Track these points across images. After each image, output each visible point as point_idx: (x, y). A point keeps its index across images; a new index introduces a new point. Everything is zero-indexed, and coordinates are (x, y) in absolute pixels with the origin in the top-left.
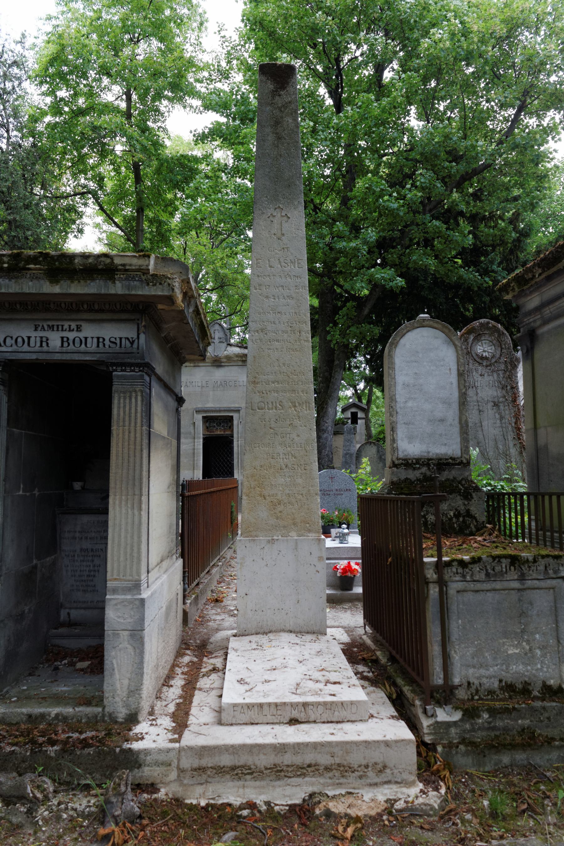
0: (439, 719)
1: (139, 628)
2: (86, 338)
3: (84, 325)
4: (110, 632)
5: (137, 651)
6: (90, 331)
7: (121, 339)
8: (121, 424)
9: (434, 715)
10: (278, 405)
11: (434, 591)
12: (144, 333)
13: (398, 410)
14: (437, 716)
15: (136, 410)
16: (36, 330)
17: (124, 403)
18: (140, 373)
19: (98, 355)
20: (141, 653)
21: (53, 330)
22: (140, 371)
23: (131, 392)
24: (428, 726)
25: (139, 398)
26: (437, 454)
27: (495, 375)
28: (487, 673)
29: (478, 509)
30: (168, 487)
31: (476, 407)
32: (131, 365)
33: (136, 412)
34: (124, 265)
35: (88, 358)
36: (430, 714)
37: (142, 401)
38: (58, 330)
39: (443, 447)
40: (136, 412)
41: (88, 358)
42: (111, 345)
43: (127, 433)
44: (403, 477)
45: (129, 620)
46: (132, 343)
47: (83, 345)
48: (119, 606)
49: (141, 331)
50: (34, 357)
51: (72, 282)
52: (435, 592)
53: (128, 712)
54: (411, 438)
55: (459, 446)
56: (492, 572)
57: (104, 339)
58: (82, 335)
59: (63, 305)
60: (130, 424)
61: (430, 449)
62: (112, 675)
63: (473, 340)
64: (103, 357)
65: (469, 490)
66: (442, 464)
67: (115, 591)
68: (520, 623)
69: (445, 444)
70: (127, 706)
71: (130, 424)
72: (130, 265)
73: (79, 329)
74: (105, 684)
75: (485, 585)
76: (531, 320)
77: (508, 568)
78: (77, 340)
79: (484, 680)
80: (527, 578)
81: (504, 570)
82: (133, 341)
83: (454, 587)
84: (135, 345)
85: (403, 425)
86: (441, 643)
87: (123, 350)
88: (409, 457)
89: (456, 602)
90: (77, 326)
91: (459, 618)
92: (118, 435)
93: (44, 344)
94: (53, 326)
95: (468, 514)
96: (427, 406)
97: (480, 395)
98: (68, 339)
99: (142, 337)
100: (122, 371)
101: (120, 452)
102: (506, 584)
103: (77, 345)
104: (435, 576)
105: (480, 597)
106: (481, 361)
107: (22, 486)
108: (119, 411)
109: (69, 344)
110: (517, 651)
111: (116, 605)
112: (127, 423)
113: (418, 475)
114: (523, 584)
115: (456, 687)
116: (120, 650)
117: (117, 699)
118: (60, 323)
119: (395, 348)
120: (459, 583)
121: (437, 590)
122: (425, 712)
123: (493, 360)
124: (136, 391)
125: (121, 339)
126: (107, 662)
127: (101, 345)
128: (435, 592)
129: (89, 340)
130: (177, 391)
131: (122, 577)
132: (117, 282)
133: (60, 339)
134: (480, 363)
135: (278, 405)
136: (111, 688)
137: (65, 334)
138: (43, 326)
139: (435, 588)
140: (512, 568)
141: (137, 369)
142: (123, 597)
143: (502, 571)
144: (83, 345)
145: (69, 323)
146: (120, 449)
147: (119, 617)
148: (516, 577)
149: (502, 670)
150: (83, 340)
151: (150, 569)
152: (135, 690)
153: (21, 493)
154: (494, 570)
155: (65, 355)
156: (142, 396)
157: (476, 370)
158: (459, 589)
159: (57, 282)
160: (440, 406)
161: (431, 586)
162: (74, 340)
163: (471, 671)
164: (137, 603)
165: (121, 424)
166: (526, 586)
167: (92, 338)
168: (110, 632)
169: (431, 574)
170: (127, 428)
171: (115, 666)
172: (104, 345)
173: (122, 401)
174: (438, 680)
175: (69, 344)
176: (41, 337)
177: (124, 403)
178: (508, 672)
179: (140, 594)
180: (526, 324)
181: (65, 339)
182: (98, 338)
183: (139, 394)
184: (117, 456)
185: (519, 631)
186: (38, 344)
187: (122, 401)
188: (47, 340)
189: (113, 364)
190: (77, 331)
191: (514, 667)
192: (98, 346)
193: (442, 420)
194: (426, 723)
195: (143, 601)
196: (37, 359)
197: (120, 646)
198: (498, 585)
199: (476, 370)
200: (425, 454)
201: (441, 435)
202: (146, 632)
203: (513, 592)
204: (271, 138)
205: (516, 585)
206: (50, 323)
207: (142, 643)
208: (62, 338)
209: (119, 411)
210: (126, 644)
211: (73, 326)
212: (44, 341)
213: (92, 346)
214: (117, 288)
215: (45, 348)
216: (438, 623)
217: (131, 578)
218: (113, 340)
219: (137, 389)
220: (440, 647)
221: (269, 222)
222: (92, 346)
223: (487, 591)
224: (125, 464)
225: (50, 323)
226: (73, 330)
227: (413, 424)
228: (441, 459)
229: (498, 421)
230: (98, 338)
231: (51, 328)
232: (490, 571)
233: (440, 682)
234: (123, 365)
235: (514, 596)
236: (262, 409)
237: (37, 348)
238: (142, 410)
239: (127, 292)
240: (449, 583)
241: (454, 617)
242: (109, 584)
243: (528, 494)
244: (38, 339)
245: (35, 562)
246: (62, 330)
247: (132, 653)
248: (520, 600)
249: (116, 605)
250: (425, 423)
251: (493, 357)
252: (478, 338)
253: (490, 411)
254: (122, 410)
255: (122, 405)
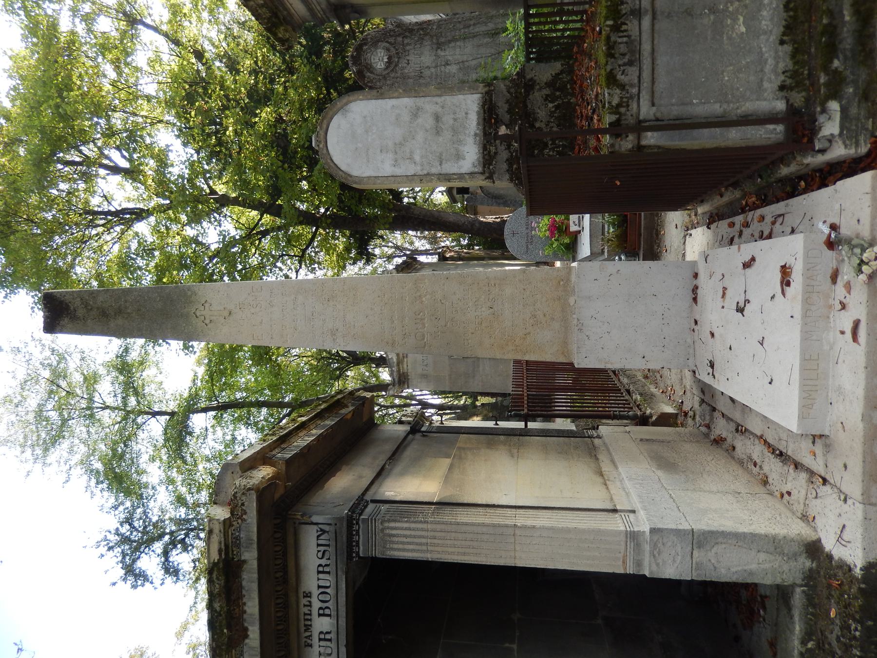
0: (836, 131)
1: (690, 536)
2: (319, 587)
3: (304, 588)
4: (694, 574)
5: (720, 540)
6: (311, 581)
7: (318, 545)
8: (424, 548)
9: (830, 140)
10: (419, 317)
11: (651, 139)
12: (310, 517)
13: (425, 172)
14: (832, 135)
15: (406, 529)
16: (311, 646)
17: (397, 543)
18: (360, 523)
19: (339, 573)
20: (724, 534)
21: (311, 625)
22: (357, 523)
23: (385, 535)
24: (846, 147)
25: (392, 525)
26: (478, 124)
27: (408, 48)
28: (770, 61)
29: (545, 72)
30: (512, 456)
31: (443, 68)
32: (350, 536)
33: (409, 529)
34: (220, 551)
35: (343, 586)
36: (827, 144)
37: (395, 521)
38: (310, 620)
39: (469, 116)
40: (409, 529)
41: (344, 586)
42: (327, 556)
43: (436, 541)
44: (505, 166)
45: (679, 549)
46: (324, 532)
47: (328, 590)
48: (660, 561)
49: (308, 521)
50: (343, 650)
51: (245, 612)
52: (652, 137)
53: (804, 555)
54: (459, 157)
55: (469, 96)
56: (627, 57)
57: (320, 565)
58: (315, 592)
59: (279, 614)
60: (423, 537)
61: (473, 133)
62: (751, 573)
63: (372, 73)
64: (342, 567)
65: (522, 84)
66: (489, 115)
67: (639, 564)
68: (701, 14)
69: (466, 114)
70: (795, 556)
71: (423, 537)
72: (220, 543)
73: (308, 595)
74: (765, 582)
75: (645, 67)
76: (318, 8)
77: (622, 34)
78: (322, 597)
79: (781, 66)
80: (637, 7)
81: (625, 39)
82: (321, 530)
83: (646, 110)
84: (326, 528)
85: (443, 166)
86: (725, 129)
87: (333, 543)
88: (481, 160)
89: (671, 109)
90: (304, 597)
91: (691, 103)
92: (438, 552)
93: (328, 636)
94: (305, 625)
95: (550, 84)
96: (420, 136)
97: (429, 64)
98: (320, 608)
99: (315, 519)
100: (358, 545)
101: (460, 550)
102: (646, 37)
103: (327, 598)
104: (631, 137)
105: (660, 71)
106: (394, 64)
107: (507, 645)
108: (408, 550)
109: (327, 608)
110: (741, 19)
111: (658, 565)
112: (424, 541)
113: (503, 148)
114: (647, 11)
115: (790, 106)
116: (719, 562)
117: (786, 568)
118: (302, 617)
119: (351, 176)
120: (641, 103)
121: (649, 134)
122: (823, 151)
123: (393, 51)
124: (382, 530)
125: (318, 545)
126: (734, 579)
127: (327, 569)
128: (652, 137)
129: (322, 583)
130: (403, 435)
131: (622, 554)
132: (243, 558)
133: (321, 618)
134: (396, 65)
135: (419, 317)
136: (769, 575)
137: (315, 612)
138: (306, 637)
139: (646, 137)
140: (624, 27)
141: (356, 527)
142: (647, 554)
143: (626, 43)
144: (328, 590)
145: (302, 606)
146: (457, 550)
147: (674, 561)
148: (636, 22)
149: (767, 40)
150: (321, 590)
151: (610, 507)
152: (774, 544)
153: (515, 646)
154: (624, 55)
155: (340, 613)
156: (389, 521)
157: (403, 68)
158: (650, 104)
159: (246, 630)
160: (420, 120)
161: (644, 142)
162: (322, 601)
163: (766, 85)
164: (655, 538)
165: (424, 548)
166: (649, 7)
167: (318, 579)
168: (694, 574)
169: (627, 144)
170: (429, 541)
171: (740, 568)
172: (326, 565)
173: (396, 546)
174: (775, 132)
175: (327, 608)
176: (320, 640)
177: (397, 543)
178: (771, 31)
179: (644, 532)
180: (325, 14)
181: (321, 612)
182: (319, 572)
183: (386, 525)
184: (464, 554)
185: (712, 17)
186: (328, 643)
187: (396, 546)
188: (321, 633)
189: (349, 557)
190: (310, 597)
191: (763, 22)
192: (328, 573)
193: (437, 118)
194: (839, 151)
195: (653, 531)
196: (346, 646)
197: (713, 561)
198: (646, 47)
199: (403, 68)
200: (478, 138)
201: (455, 120)
202: (697, 527)
203: (657, 27)
204: (120, 321)
205: (646, 22)
206: (303, 629)
207: (712, 533)
208: (320, 615)
209: (408, 550)
210: (711, 555)
211: (304, 601)
212: (324, 637)
213: (328, 580)
214: (250, 556)
215: (333, 636)
216: (696, 132)
217: (623, 544)
218: (320, 555)
219: (381, 527)
220: (731, 129)
221: (212, 324)
222: (328, 580)
223: (653, 63)
224: (475, 544)
225: (303, 629)
226: (310, 602)
227: (441, 154)
228: (484, 119)
229: (458, 43)
230: (319, 572)
231: (308, 628)
232: (626, 60)
233: (780, 128)
234: (351, 544)
235: (662, 25)
236: (424, 335)
237: (333, 645)
238: (406, 522)
239: (255, 546)
240: (641, 118)
241: (689, 110)
242: (630, 570)
243: (527, 8)
244: (322, 643)
245: (600, 621)
246: (310, 615)
247: (724, 546)
248: (669, 16)
249: (658, 565)
250: (441, 139)
251: (388, 50)
252: (370, 68)
253: (447, 53)
254: (406, 547)
255: (401, 546)
